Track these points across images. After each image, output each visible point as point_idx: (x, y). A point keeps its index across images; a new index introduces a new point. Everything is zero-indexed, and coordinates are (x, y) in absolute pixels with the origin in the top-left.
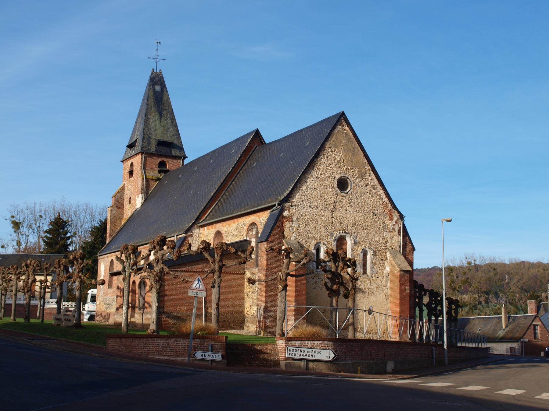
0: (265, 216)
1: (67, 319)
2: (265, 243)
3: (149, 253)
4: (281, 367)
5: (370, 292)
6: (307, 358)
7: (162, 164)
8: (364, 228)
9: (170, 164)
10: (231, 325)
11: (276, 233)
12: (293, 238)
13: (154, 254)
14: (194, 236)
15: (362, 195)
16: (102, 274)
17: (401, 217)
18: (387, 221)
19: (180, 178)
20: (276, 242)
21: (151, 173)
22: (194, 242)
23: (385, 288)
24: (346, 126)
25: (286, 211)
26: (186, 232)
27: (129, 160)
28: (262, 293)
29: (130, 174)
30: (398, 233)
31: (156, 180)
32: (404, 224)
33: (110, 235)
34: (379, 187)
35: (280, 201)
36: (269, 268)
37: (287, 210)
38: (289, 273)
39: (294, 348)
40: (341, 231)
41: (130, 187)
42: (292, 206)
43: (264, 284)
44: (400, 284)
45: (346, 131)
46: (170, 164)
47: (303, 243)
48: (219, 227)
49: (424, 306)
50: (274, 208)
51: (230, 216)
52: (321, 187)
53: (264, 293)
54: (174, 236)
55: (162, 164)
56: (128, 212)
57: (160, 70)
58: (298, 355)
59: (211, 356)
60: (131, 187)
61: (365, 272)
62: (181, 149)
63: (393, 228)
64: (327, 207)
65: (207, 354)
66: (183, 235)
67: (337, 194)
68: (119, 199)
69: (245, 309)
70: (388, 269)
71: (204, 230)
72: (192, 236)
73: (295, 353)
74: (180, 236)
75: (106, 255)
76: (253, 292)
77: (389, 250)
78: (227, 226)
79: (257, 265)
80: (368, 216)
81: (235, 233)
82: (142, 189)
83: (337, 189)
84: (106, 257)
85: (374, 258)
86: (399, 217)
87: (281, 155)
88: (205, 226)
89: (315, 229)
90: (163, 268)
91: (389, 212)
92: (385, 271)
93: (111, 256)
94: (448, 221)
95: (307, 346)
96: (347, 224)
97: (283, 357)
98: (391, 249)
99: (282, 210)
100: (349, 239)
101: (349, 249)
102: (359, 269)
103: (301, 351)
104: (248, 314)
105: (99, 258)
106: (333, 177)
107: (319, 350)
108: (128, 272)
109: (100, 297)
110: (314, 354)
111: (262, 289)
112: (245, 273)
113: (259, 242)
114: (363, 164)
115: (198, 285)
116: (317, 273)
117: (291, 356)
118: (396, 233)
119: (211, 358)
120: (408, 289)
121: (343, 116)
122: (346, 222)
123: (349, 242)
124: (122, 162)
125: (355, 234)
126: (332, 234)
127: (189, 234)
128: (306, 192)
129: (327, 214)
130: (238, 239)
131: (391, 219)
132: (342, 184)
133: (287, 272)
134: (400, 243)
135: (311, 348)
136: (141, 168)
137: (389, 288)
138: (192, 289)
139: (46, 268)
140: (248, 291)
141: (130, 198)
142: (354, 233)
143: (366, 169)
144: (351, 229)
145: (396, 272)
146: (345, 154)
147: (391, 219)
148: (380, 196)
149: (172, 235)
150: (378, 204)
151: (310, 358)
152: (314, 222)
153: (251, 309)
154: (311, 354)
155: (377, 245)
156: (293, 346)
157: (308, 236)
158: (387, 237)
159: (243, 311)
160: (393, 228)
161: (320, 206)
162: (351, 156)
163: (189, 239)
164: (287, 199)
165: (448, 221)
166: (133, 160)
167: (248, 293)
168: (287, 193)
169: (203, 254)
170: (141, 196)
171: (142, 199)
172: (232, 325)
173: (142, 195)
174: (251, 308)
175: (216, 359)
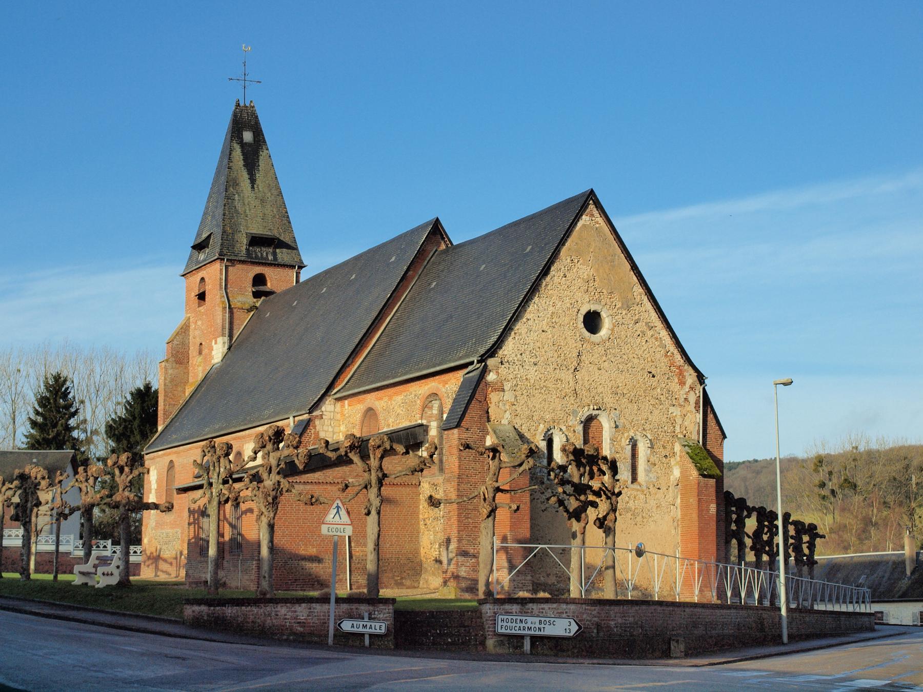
0: (453, 381)
1: (106, 573)
2: (456, 431)
3: (254, 456)
4: (487, 649)
5: (644, 515)
6: (532, 632)
7: (259, 280)
8: (632, 400)
9: (277, 280)
10: (396, 578)
11: (474, 411)
12: (505, 422)
13: (264, 458)
14: (324, 417)
15: (629, 341)
16: (153, 487)
17: (701, 378)
18: (674, 385)
19: (295, 307)
20: (475, 429)
21: (240, 298)
22: (325, 428)
23: (672, 507)
24: (599, 216)
25: (491, 373)
26: (311, 411)
27: (198, 272)
28: (452, 521)
29: (198, 298)
30: (695, 407)
31: (249, 310)
32: (704, 390)
33: (164, 414)
34: (659, 324)
35: (482, 356)
36: (463, 476)
37: (494, 371)
38: (498, 487)
39: (510, 618)
40: (592, 407)
41: (199, 323)
42: (502, 363)
43: (455, 506)
44: (699, 501)
45: (597, 225)
46: (277, 280)
47: (524, 430)
48: (371, 400)
49: (746, 538)
50: (470, 368)
51: (392, 381)
52: (554, 327)
53: (454, 520)
54: (289, 418)
55: (259, 280)
56: (198, 371)
57: (251, 102)
58: (516, 628)
59: (368, 627)
60: (202, 324)
61: (634, 479)
62: (291, 247)
63: (686, 399)
64: (565, 363)
65: (361, 624)
66: (306, 417)
67: (583, 339)
68: (180, 347)
69: (422, 549)
70: (677, 473)
71: (343, 406)
72: (321, 417)
73: (511, 625)
74: (301, 418)
75: (160, 453)
76: (436, 519)
77: (679, 439)
78: (386, 399)
79: (441, 470)
80: (639, 377)
81: (401, 412)
82: (223, 328)
83: (584, 330)
84: (159, 457)
85: (652, 453)
86: (696, 379)
87: (482, 268)
88: (346, 399)
89: (544, 403)
90: (279, 482)
91: (678, 371)
92: (671, 477)
93: (169, 454)
94: (785, 384)
95: (532, 612)
96: (602, 393)
97: (491, 631)
98: (682, 436)
99: (485, 371)
100: (606, 420)
101: (606, 439)
102: (624, 474)
103: (521, 621)
104: (426, 559)
105: (146, 457)
106: (576, 310)
107: (552, 620)
108: (216, 489)
109: (150, 530)
110: (544, 626)
111: (451, 514)
112: (420, 485)
113: (446, 427)
114: (630, 283)
115: (337, 515)
116: (548, 482)
117: (503, 631)
118: (691, 407)
119: (368, 630)
120: (713, 508)
121: (591, 199)
122: (600, 389)
123: (605, 423)
124: (183, 276)
125: (617, 412)
126: (575, 413)
127: (314, 414)
128: (526, 338)
129: (567, 376)
130: (405, 424)
131: (682, 383)
132: (592, 321)
133: (496, 486)
134: (699, 426)
135: (538, 616)
136: (221, 288)
137: (679, 508)
138: (328, 522)
139: (60, 482)
140: (426, 516)
141: (201, 344)
142: (616, 409)
143: (635, 294)
144: (609, 400)
145: (691, 478)
146: (597, 266)
147: (682, 383)
148: (661, 341)
149: (286, 417)
150: (658, 356)
151: (537, 633)
152: (543, 391)
153: (433, 549)
154: (537, 625)
155: (656, 430)
156: (507, 613)
157: (533, 416)
158: (674, 414)
159: (416, 552)
160: (686, 399)
161: (552, 363)
162: (607, 271)
163: (317, 422)
164: (492, 352)
165: (785, 384)
166: (205, 272)
167: (427, 520)
168: (494, 339)
169: (348, 457)
170: (222, 342)
171: (224, 347)
172: (399, 578)
173: (223, 339)
174: (431, 548)
175: (376, 631)
